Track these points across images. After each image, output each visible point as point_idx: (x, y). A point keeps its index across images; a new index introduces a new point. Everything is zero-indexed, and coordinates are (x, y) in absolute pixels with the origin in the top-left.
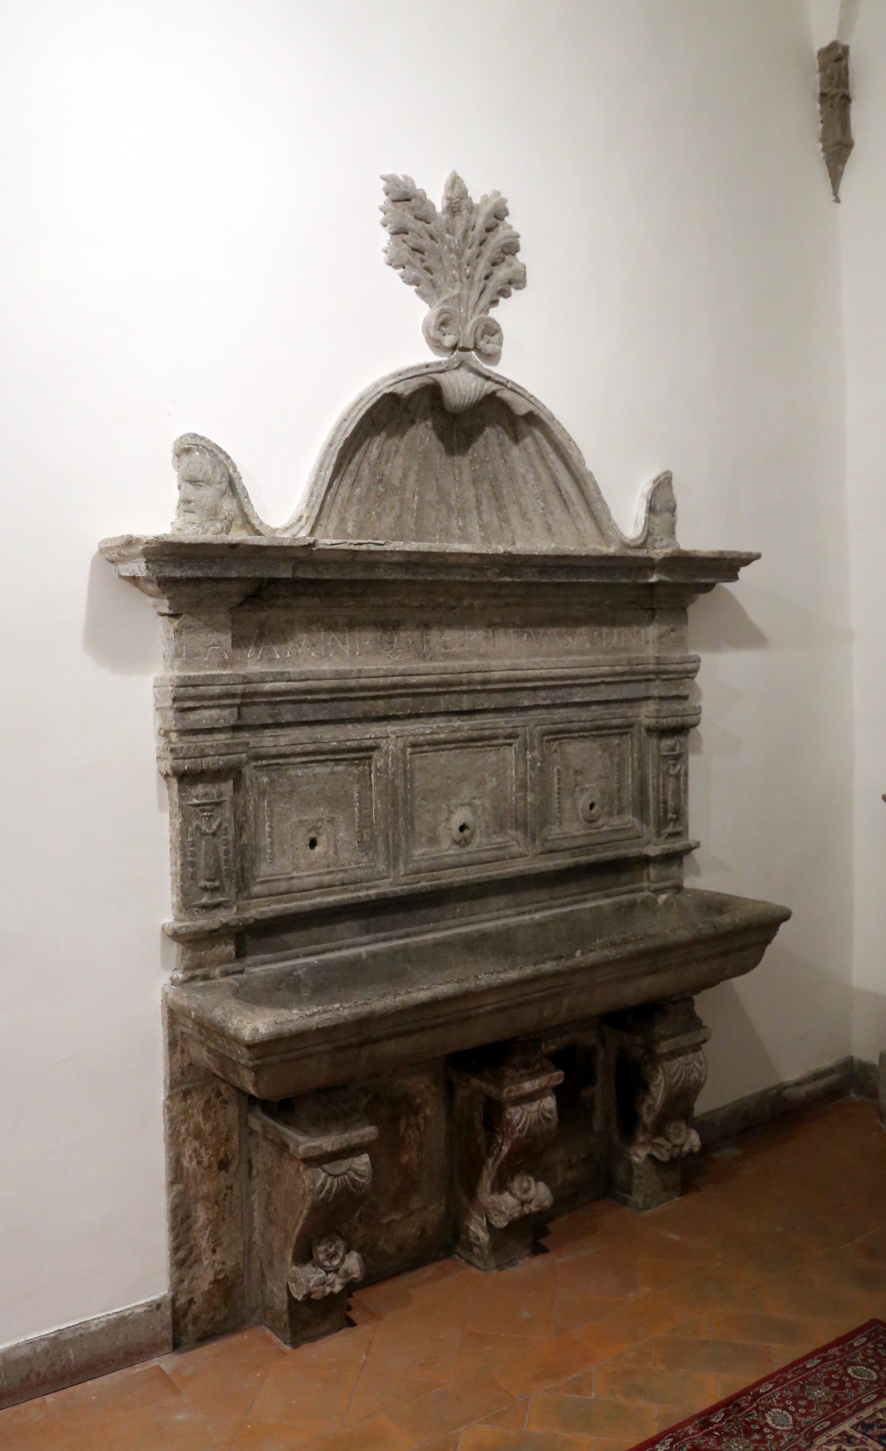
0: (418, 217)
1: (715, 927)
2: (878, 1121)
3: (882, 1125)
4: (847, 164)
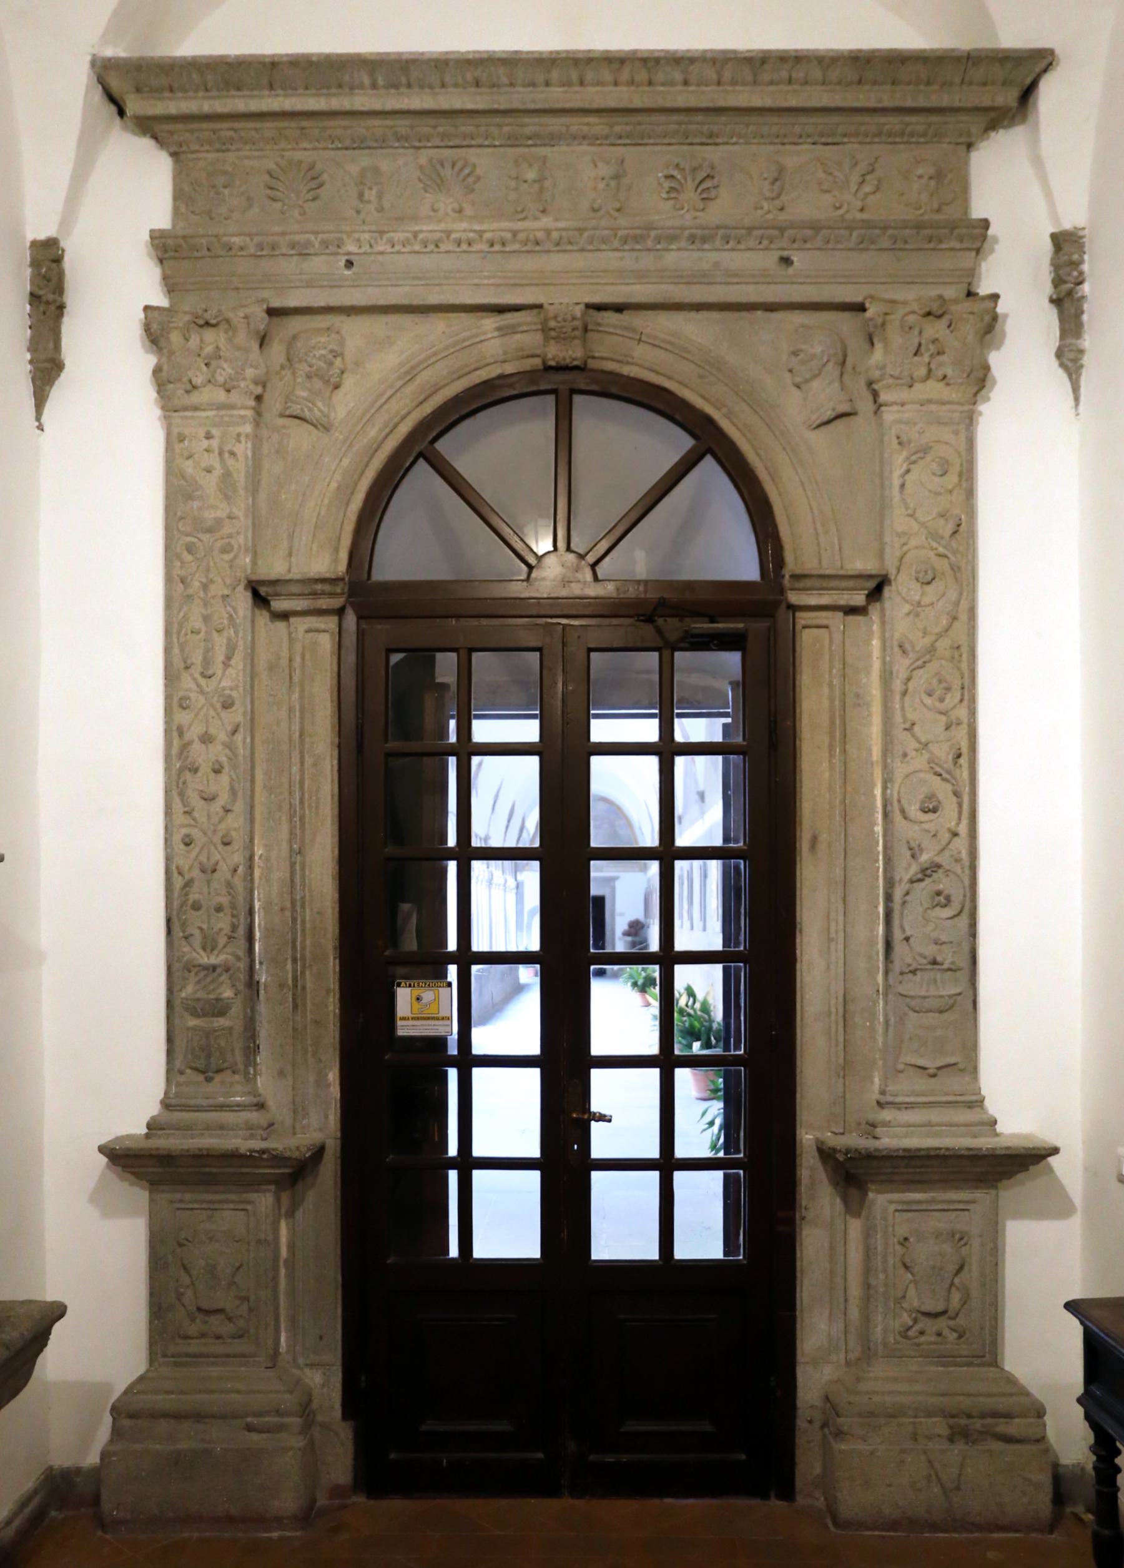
0: (113, 109)
1: (7, 1348)
2: (100, 1533)
3: (108, 1537)
4: (55, 387)
